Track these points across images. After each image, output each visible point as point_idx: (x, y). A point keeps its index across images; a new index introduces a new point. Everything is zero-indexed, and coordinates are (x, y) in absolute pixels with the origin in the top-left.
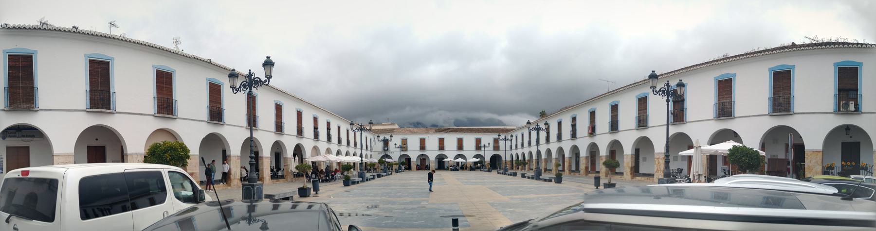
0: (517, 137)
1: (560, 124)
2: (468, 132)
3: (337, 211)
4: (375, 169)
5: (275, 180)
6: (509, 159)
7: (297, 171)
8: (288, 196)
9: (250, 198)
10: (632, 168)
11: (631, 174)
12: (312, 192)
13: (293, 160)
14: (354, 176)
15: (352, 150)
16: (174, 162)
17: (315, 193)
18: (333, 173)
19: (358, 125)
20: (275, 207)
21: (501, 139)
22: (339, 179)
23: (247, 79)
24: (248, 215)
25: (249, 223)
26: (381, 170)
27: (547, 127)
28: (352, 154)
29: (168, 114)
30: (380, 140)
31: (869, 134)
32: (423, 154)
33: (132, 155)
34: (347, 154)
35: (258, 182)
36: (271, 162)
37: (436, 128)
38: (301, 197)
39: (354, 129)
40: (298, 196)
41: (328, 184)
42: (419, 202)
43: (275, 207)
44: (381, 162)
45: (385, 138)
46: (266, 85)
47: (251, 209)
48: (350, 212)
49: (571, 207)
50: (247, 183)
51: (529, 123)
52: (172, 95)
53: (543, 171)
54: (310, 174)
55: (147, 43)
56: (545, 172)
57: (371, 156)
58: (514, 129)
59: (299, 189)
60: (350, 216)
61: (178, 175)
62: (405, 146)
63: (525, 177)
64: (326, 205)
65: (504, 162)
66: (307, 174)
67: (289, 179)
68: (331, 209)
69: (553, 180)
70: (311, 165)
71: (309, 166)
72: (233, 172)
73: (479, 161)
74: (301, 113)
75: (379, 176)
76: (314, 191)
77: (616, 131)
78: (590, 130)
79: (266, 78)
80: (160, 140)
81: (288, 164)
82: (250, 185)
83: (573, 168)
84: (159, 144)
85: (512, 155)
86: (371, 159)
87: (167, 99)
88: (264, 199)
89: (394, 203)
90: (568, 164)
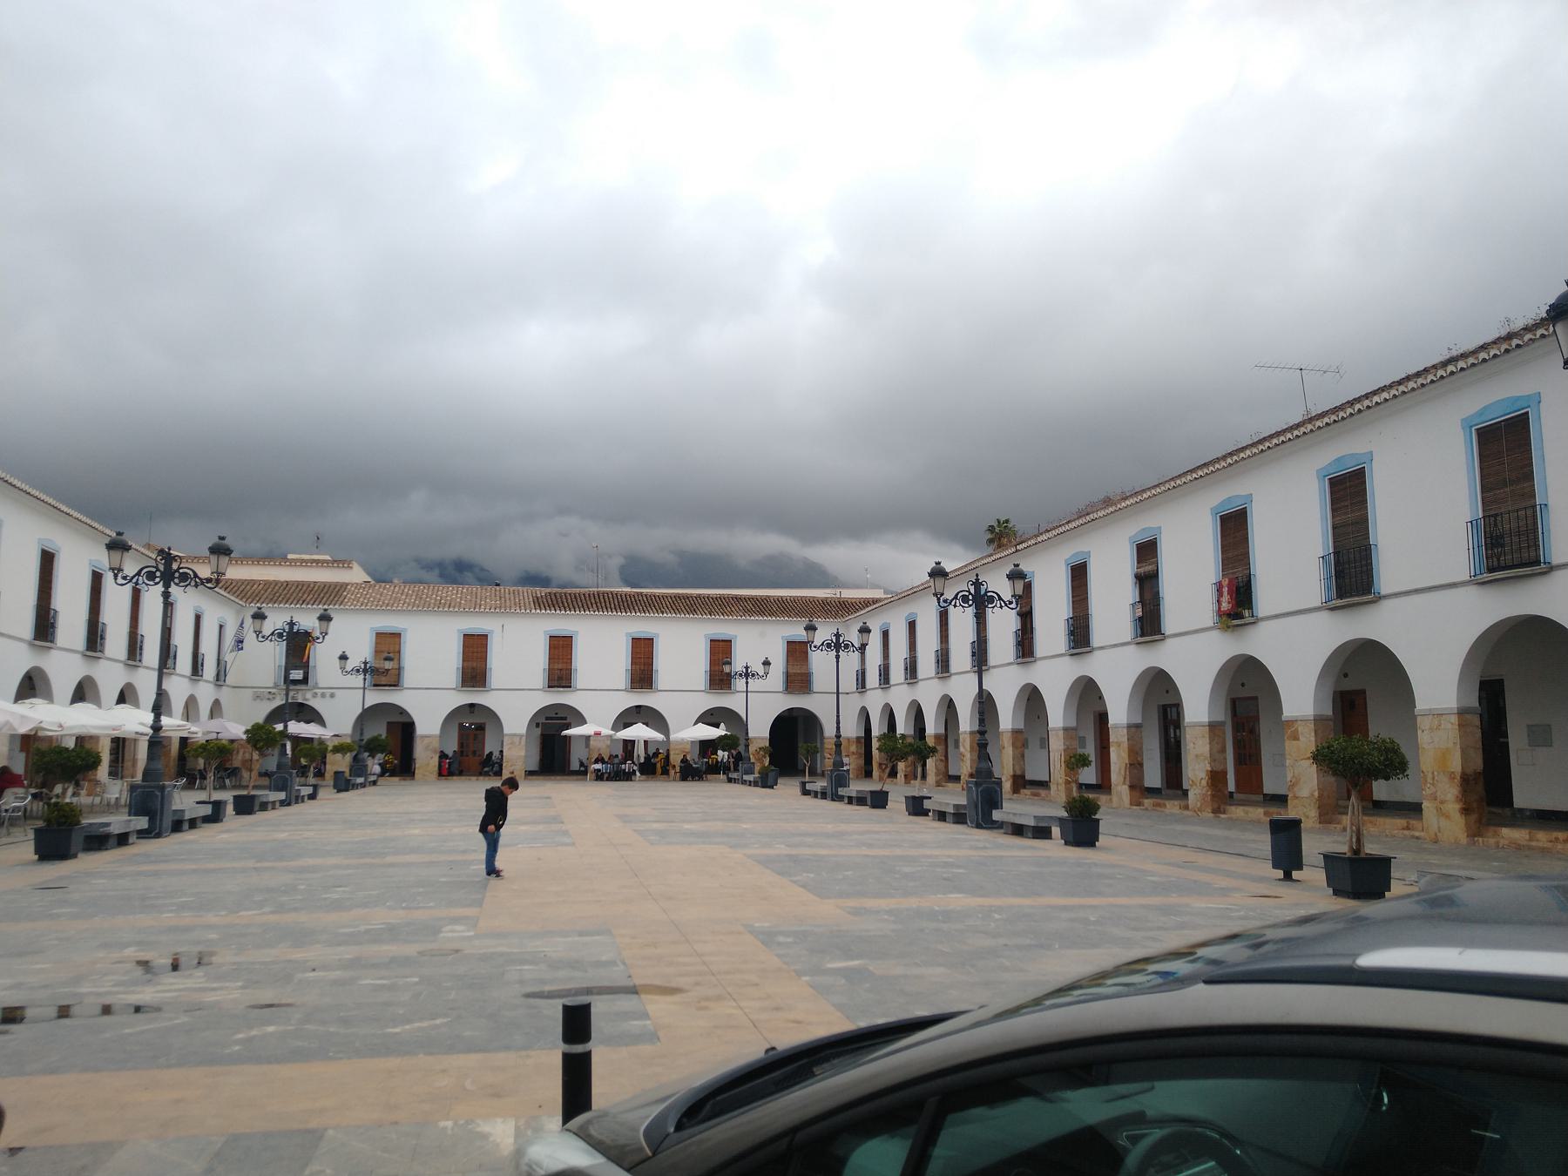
0: (885, 634)
1: (1079, 574)
6: (851, 729)
10: (1466, 781)
11: (1466, 811)
14: (111, 808)
21: (817, 642)
26: (266, 774)
27: (1019, 591)
31: (664, 715)
32: (472, 705)
34: (84, 692)
37: (541, 591)
39: (130, 569)
44: (261, 737)
45: (291, 624)
49: (1147, 960)
51: (938, 573)
53: (1007, 785)
56: (1016, 790)
57: (216, 709)
58: (875, 601)
62: (388, 665)
63: (925, 813)
65: (829, 744)
69: (1056, 831)
73: (721, 738)
75: (245, 806)
77: (1365, 598)
78: (1226, 597)
83: (1153, 777)
85: (865, 716)
89: (301, 937)
90: (1125, 755)
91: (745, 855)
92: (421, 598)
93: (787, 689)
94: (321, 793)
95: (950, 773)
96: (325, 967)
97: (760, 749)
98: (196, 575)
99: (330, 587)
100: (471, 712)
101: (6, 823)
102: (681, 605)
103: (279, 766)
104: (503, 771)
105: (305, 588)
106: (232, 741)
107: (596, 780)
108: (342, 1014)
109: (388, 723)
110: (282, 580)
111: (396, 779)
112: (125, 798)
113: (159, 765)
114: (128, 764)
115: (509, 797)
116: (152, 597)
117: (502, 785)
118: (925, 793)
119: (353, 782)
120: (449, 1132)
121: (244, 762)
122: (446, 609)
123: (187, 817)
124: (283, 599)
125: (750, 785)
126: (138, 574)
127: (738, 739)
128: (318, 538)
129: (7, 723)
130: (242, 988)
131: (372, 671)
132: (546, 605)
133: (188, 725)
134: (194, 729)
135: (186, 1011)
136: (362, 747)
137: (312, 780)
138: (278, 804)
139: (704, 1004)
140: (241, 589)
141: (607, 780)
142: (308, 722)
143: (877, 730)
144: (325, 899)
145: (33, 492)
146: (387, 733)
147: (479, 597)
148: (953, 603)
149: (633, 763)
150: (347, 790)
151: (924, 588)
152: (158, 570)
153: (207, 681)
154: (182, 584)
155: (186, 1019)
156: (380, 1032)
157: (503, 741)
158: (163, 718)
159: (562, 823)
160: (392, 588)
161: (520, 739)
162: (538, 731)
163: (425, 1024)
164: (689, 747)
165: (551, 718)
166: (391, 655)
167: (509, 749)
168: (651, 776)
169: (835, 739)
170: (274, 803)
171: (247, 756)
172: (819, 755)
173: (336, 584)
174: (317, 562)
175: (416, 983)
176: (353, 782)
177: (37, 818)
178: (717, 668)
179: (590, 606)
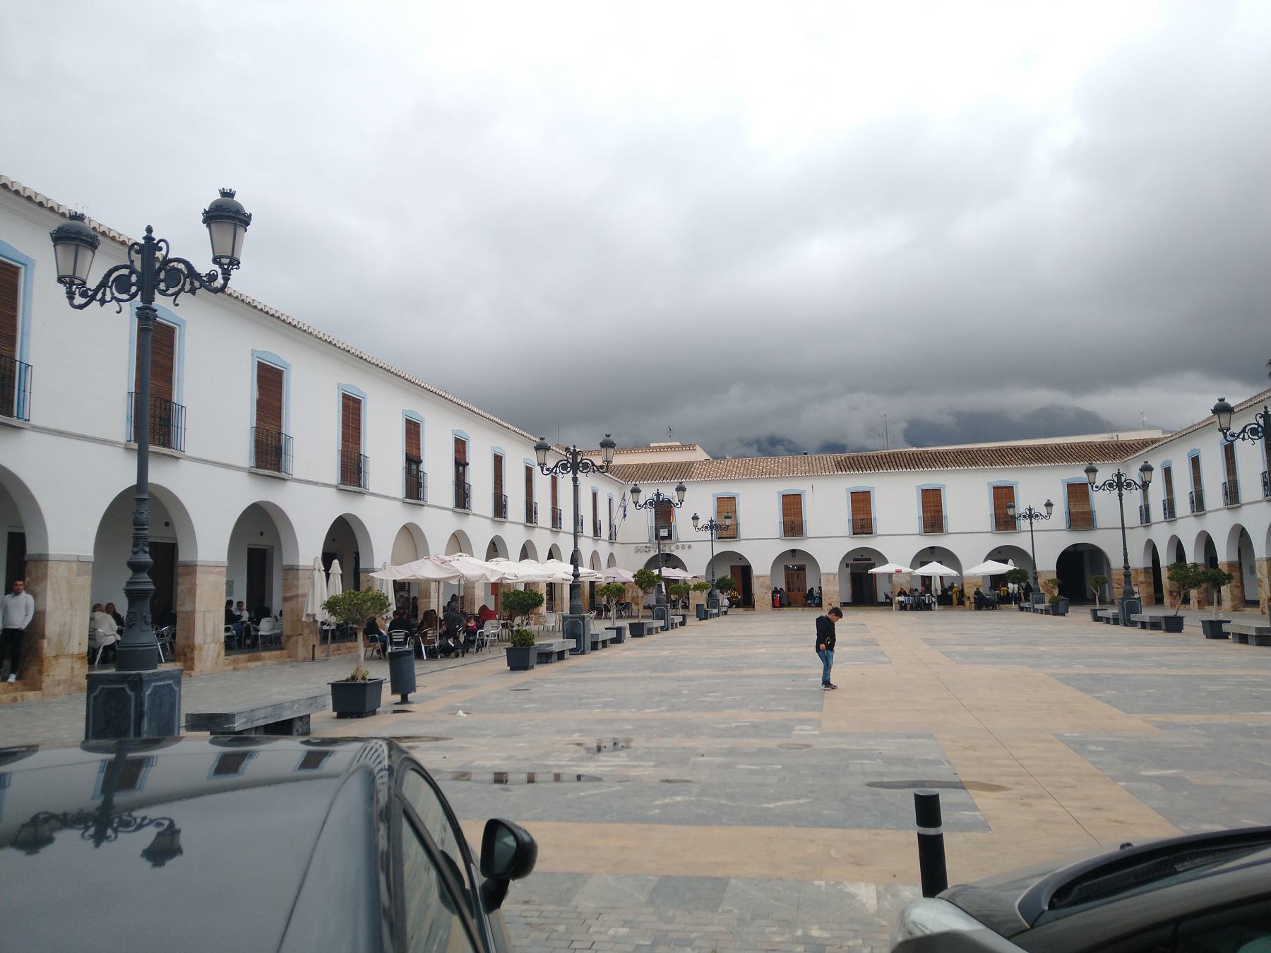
0: (1168, 472)
2: (959, 463)
3: (475, 764)
4: (627, 606)
6: (1139, 560)
7: (333, 619)
8: (287, 716)
12: (388, 696)
13: (320, 576)
14: (550, 633)
17: (398, 698)
18: (472, 624)
21: (1099, 482)
22: (492, 644)
26: (647, 607)
28: (543, 552)
30: (642, 502)
32: (793, 551)
36: (230, 584)
37: (841, 456)
39: (551, 464)
40: (329, 711)
42: (786, 728)
44: (644, 579)
45: (658, 495)
46: (216, 291)
50: (112, 671)
51: (1222, 409)
57: (611, 561)
58: (1154, 441)
59: (337, 688)
62: (728, 522)
63: (1225, 636)
67: (301, 652)
72: (52, 627)
73: (1010, 572)
74: (358, 402)
75: (638, 631)
76: (394, 692)
79: (216, 267)
81: (300, 592)
82: (124, 679)
85: (1152, 548)
86: (612, 569)
88: (183, 733)
89: (691, 730)
91: (1045, 674)
93: (1070, 527)
94: (688, 621)
95: (1246, 599)
96: (711, 754)
97: (1048, 581)
98: (593, 464)
101: (488, 645)
102: (963, 458)
103: (658, 601)
104: (823, 603)
106: (624, 583)
107: (901, 610)
108: (728, 791)
109: (731, 566)
111: (741, 610)
112: (559, 626)
113: (578, 602)
114: (558, 602)
115: (835, 624)
116: (565, 481)
117: (829, 614)
118: (1221, 617)
119: (710, 612)
121: (633, 598)
122: (767, 476)
125: (1042, 613)
126: (556, 466)
127: (1027, 573)
130: (654, 766)
132: (846, 467)
133: (595, 572)
134: (599, 575)
137: (681, 611)
138: (659, 629)
139: (1026, 801)
140: (621, 472)
141: (911, 610)
142: (674, 568)
143: (1165, 560)
144: (703, 701)
148: (1241, 436)
149: (932, 596)
151: (1205, 426)
152: (568, 462)
154: (584, 471)
156: (758, 806)
157: (820, 580)
158: (579, 568)
159: (878, 645)
161: (834, 577)
162: (849, 570)
163: (792, 802)
164: (980, 581)
165: (858, 560)
166: (730, 514)
167: (827, 585)
168: (948, 606)
169: (1124, 571)
170: (657, 628)
171: (635, 594)
172: (1107, 585)
173: (685, 463)
174: (671, 447)
175: (779, 770)
176: (710, 612)
177: (506, 641)
178: (1001, 511)
179: (883, 466)
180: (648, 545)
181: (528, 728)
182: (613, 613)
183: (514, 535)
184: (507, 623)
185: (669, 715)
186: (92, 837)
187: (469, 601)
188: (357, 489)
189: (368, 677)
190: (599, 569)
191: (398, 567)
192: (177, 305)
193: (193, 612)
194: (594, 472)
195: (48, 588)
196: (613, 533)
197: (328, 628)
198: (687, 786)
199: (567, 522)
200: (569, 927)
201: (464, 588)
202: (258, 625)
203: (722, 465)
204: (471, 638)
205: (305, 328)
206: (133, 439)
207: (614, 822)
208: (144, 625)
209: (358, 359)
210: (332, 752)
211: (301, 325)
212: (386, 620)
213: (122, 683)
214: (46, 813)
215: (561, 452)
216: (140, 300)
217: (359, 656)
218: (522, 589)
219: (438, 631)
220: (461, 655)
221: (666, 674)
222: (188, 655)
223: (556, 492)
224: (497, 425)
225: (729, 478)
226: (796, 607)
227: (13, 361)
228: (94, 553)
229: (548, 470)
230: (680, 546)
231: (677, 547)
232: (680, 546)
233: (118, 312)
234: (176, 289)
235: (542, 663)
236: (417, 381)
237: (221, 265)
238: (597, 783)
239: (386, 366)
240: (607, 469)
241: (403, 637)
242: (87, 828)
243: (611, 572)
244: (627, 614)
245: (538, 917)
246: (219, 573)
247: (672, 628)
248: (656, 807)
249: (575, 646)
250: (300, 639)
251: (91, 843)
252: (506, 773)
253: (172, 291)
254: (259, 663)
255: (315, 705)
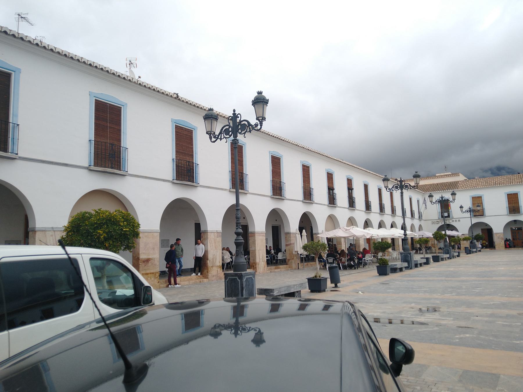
3: (369, 314)
4: (429, 248)
5: (273, 267)
7: (306, 253)
8: (292, 291)
9: (236, 295)
12: (329, 284)
14: (395, 260)
15: (388, 219)
16: (111, 243)
17: (333, 285)
18: (360, 256)
19: (396, 180)
20: (275, 308)
23: (231, 122)
24: (233, 321)
25: (236, 334)
26: (440, 249)
28: (388, 225)
29: (112, 168)
30: (434, 201)
32: (515, 221)
33: (44, 231)
34: (381, 225)
35: (248, 271)
36: (267, 240)
38: (312, 291)
39: (390, 186)
40: (307, 290)
41: (353, 271)
43: (275, 308)
44: (438, 236)
45: (442, 197)
46: (258, 130)
47: (238, 311)
48: (391, 316)
50: (232, 272)
52: (119, 140)
54: (325, 256)
55: (82, 58)
59: (309, 280)
60: (390, 323)
61: (112, 265)
62: (478, 208)
64: (352, 305)
66: (320, 257)
67: (294, 266)
68: (359, 311)
70: (326, 243)
71: (323, 245)
72: (210, 256)
74: (308, 167)
75: (436, 259)
76: (332, 282)
79: (258, 121)
80: (91, 208)
81: (292, 242)
82: (236, 275)
84: (89, 213)
87: (112, 145)
88: (257, 295)
89: (469, 305)
92: (487, 183)
94: (461, 255)
96: (481, 316)
98: (410, 185)
99: (452, 183)
100: (515, 223)
103: (445, 246)
105: (444, 185)
106: (428, 238)
108: (493, 333)
109: (482, 229)
110: (436, 183)
111: (488, 249)
116: (397, 194)
120: (133, 238)
122: (518, 183)
123: (419, 263)
124: (437, 189)
126: (393, 187)
128: (446, 167)
129: (364, 235)
131: (473, 211)
134: (415, 235)
135: (436, 326)
136: (473, 239)
137: (457, 250)
138: (447, 258)
140: (422, 188)
142: (452, 230)
145: (360, 168)
146: (482, 233)
147: (511, 179)
150: (470, 253)
152: (398, 185)
153: (416, 219)
154: (406, 189)
155: (438, 329)
158: (407, 231)
160: (476, 181)
164: (121, 251)
166: (479, 205)
170: (445, 258)
171: (433, 243)
173: (455, 182)
174: (447, 175)
180: (438, 220)
181: (391, 300)
182: (424, 250)
183: (375, 218)
184: (375, 255)
185: (457, 297)
186: (233, 333)
187: (358, 246)
188: (310, 201)
189: (321, 277)
190: (415, 231)
191: (328, 232)
192: (245, 137)
193: (255, 250)
194: (411, 189)
195: (208, 242)
196: (421, 216)
197: (303, 256)
198: (471, 330)
199: (399, 211)
200: (422, 388)
201: (355, 241)
202: (277, 255)
203: (474, 182)
204: (360, 261)
205: (287, 140)
206: (232, 188)
207: (436, 343)
208: (241, 255)
209: (307, 150)
210: (309, 304)
211: (286, 140)
212: (325, 254)
213: (236, 276)
214: (218, 324)
215: (394, 181)
216: (233, 137)
217: (317, 268)
218: (380, 241)
219: (346, 259)
220: (357, 268)
221: (453, 279)
222: (255, 266)
223: (393, 199)
224: (365, 172)
225: (468, 188)
226: (518, 247)
227: (193, 163)
228: (222, 229)
229: (389, 189)
230: (454, 221)
231: (453, 221)
232: (454, 221)
233: (226, 142)
234: (245, 131)
235: (393, 272)
236: (331, 157)
237: (259, 120)
238: (426, 326)
239: (318, 152)
240: (417, 187)
241: (332, 260)
242: (232, 330)
243: (421, 233)
244: (430, 252)
245: (407, 381)
246: (263, 236)
247: (453, 258)
248: (457, 338)
249: (407, 266)
250: (293, 261)
251: (234, 336)
252: (379, 319)
253: (243, 132)
254: (279, 270)
255: (302, 287)
